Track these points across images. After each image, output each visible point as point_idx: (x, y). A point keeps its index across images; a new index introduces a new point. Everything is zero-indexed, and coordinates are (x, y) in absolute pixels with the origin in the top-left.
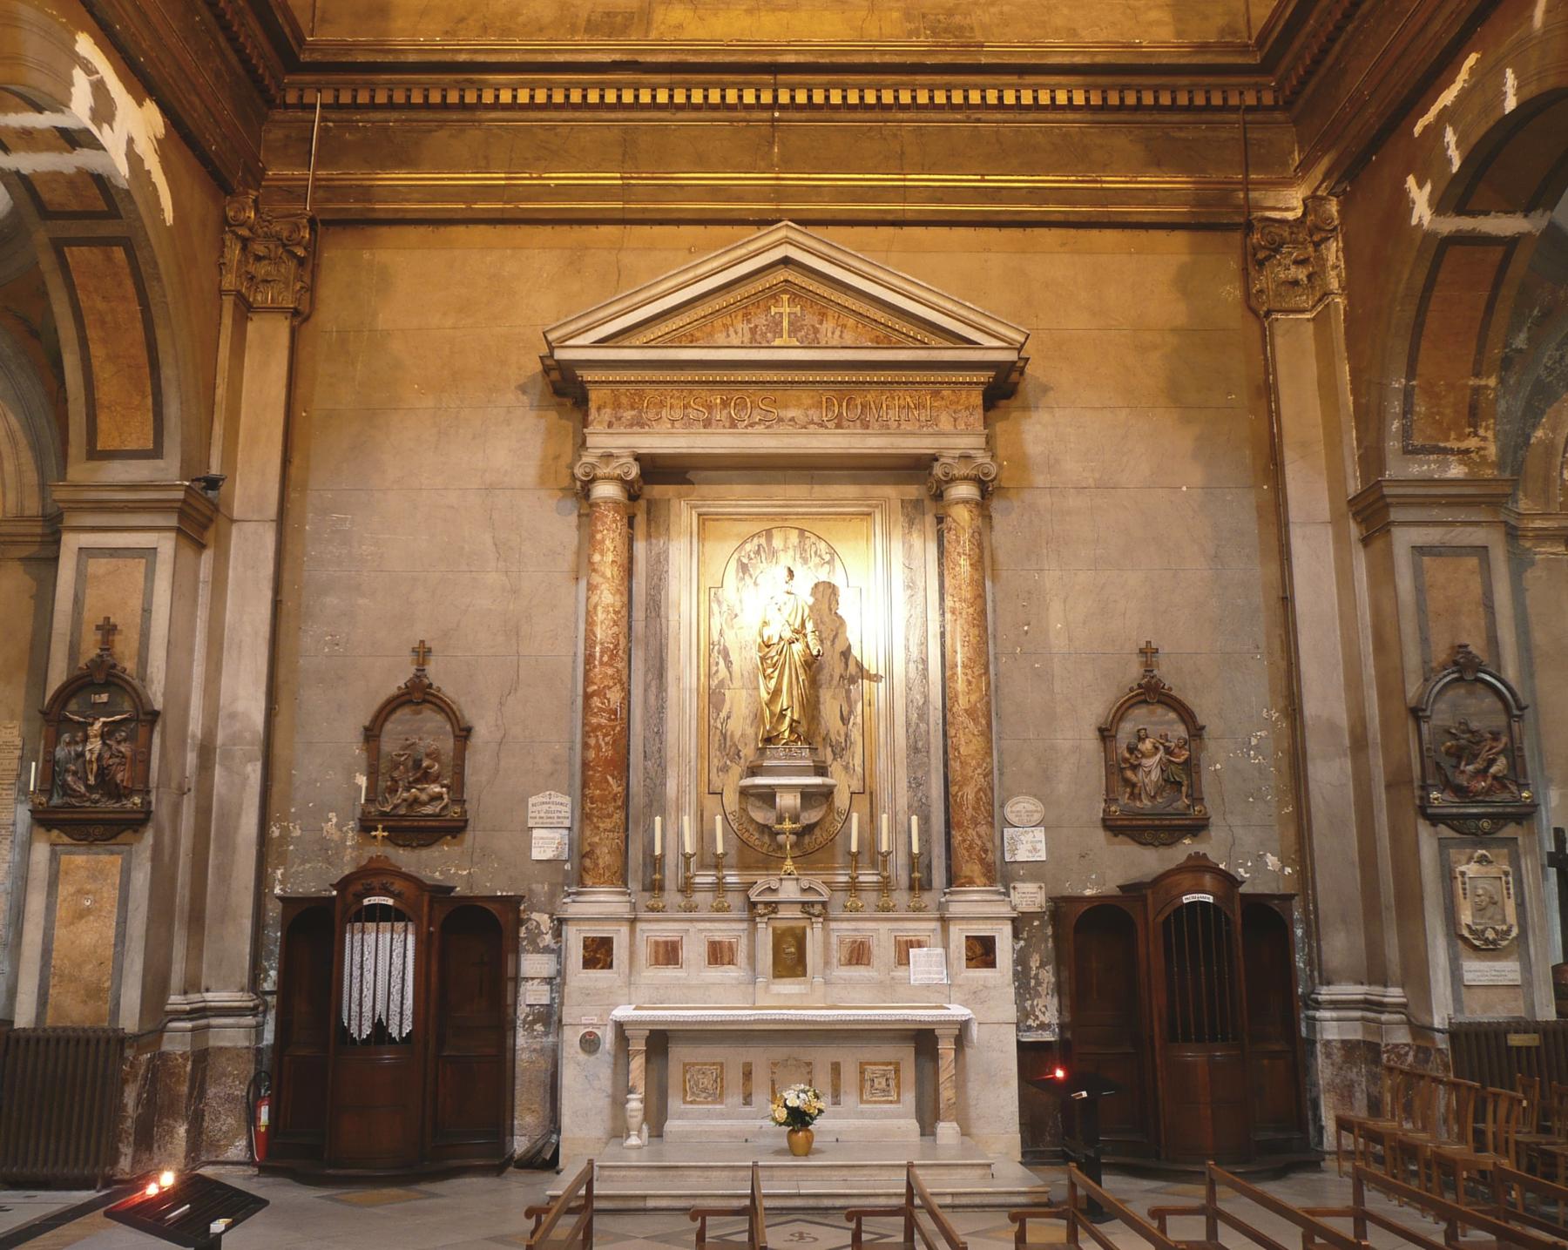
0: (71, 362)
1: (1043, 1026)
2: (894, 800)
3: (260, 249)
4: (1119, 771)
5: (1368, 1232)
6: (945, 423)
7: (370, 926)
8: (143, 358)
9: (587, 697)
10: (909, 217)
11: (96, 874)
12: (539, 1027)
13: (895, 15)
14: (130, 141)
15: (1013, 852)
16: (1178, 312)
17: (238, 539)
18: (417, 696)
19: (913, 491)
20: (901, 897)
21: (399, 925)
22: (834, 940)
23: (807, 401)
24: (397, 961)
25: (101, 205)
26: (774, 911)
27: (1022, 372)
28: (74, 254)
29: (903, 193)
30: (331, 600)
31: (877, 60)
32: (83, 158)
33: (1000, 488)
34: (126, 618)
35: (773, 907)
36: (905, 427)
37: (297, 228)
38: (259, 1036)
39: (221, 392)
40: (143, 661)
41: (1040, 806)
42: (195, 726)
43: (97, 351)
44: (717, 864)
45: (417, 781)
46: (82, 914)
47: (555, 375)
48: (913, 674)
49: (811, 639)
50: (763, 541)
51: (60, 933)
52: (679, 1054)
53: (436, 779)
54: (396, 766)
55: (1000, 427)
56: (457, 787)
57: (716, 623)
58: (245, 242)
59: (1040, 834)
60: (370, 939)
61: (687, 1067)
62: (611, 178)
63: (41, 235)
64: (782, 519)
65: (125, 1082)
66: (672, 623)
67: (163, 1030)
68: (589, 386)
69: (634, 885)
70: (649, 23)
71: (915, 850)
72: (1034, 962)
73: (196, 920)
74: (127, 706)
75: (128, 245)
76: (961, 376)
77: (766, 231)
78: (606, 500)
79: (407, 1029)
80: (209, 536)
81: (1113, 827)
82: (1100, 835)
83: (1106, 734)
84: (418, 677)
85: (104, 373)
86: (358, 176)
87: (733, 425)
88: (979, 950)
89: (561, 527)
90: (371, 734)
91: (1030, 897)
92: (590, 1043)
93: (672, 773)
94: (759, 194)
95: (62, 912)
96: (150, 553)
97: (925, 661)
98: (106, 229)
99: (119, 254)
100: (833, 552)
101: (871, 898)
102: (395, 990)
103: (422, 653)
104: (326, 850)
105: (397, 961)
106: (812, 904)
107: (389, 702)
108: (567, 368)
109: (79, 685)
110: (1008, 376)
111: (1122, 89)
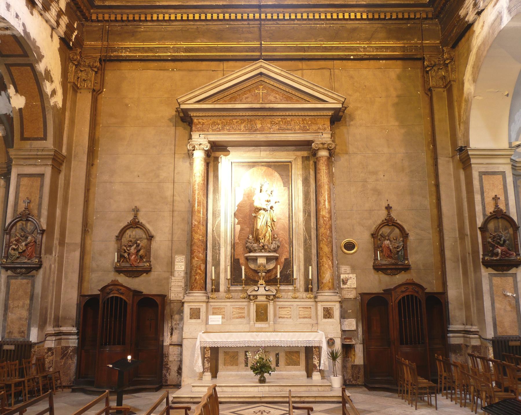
19: (305, 154)
26: (256, 298)
27: (344, 112)
35: (256, 296)
47: (182, 115)
55: (337, 131)
68: (193, 118)
71: (213, 278)
77: (251, 64)
81: (377, 268)
84: (135, 219)
90: (119, 237)
103: (136, 211)
106: (269, 296)
108: (185, 111)
110: (339, 113)
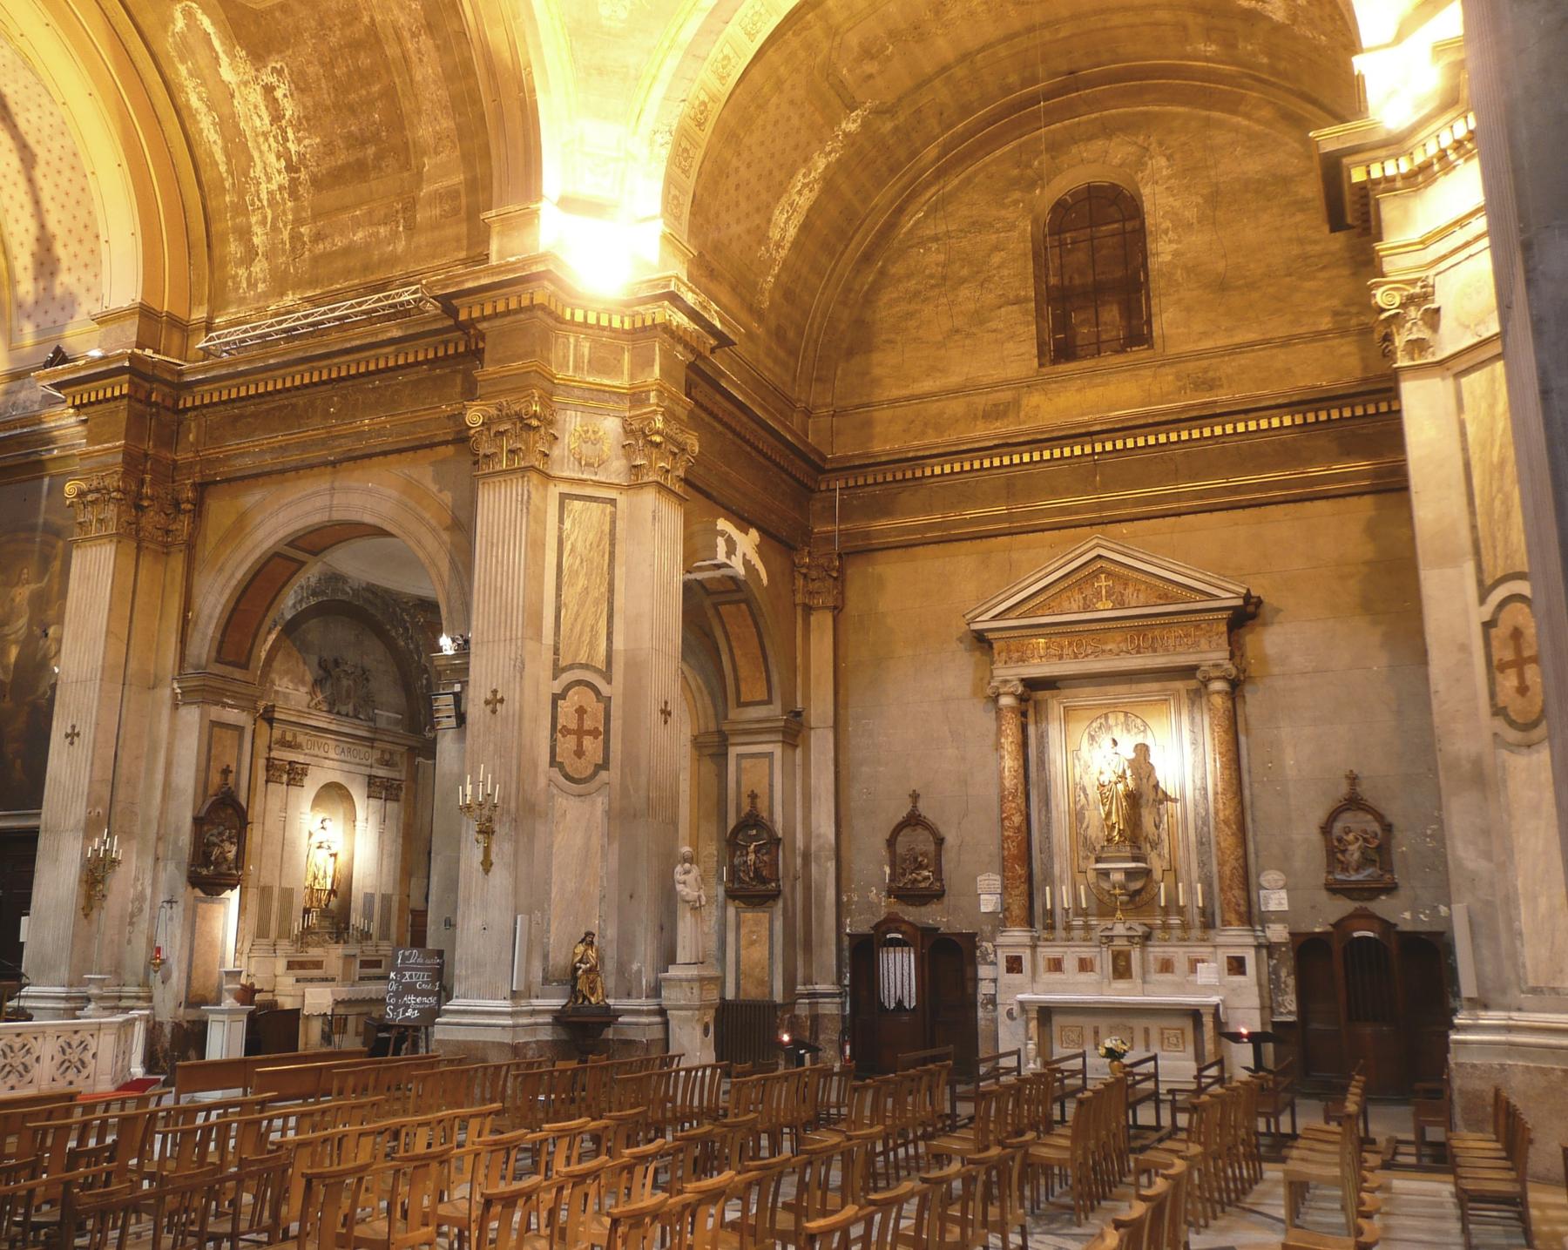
0: (725, 658)
1: (1290, 1013)
2: (1189, 872)
3: (814, 574)
4: (1334, 852)
5: (1560, 1161)
6: (1204, 643)
7: (891, 949)
8: (759, 653)
9: (1003, 820)
10: (1183, 510)
11: (758, 923)
12: (990, 1007)
13: (1171, 378)
14: (744, 555)
15: (1267, 904)
16: (1367, 551)
17: (814, 738)
18: (913, 822)
19: (1193, 684)
20: (1196, 933)
21: (906, 949)
22: (1151, 957)
23: (1119, 639)
24: (906, 967)
25: (734, 587)
28: (722, 609)
29: (1178, 497)
30: (864, 769)
31: (1150, 421)
32: (724, 571)
33: (1250, 677)
34: (761, 790)
36: (1179, 649)
37: (831, 561)
38: (843, 1009)
39: (799, 660)
40: (771, 813)
41: (1284, 877)
42: (800, 844)
43: (737, 652)
44: (1084, 913)
45: (916, 869)
46: (752, 943)
48: (1198, 797)
49: (1129, 781)
50: (1103, 720)
51: (743, 952)
52: (1058, 1021)
53: (926, 868)
54: (905, 861)
56: (938, 872)
57: (1078, 771)
58: (805, 576)
59: (1283, 894)
60: (892, 956)
61: (1062, 1028)
62: (1001, 510)
63: (707, 603)
64: (1114, 708)
65: (778, 1028)
66: (1053, 773)
67: (795, 1003)
69: (1038, 926)
70: (1019, 407)
72: (1283, 973)
73: (808, 946)
74: (765, 835)
75: (748, 602)
76: (1211, 616)
78: (1007, 707)
79: (913, 1004)
80: (799, 740)
81: (1334, 889)
82: (1324, 894)
83: (1326, 829)
85: (741, 662)
86: (862, 525)
87: (1076, 657)
88: (1235, 964)
89: (987, 721)
90: (891, 843)
91: (1277, 933)
92: (1010, 1014)
93: (1056, 860)
94: (1088, 508)
95: (743, 943)
96: (770, 755)
97: (1205, 789)
98: (736, 597)
99: (743, 606)
100: (1145, 724)
101: (1178, 933)
102: (906, 983)
103: (915, 797)
104: (872, 907)
105: (906, 967)
106: (1133, 937)
107: (894, 830)
109: (742, 826)
111: (1316, 412)
